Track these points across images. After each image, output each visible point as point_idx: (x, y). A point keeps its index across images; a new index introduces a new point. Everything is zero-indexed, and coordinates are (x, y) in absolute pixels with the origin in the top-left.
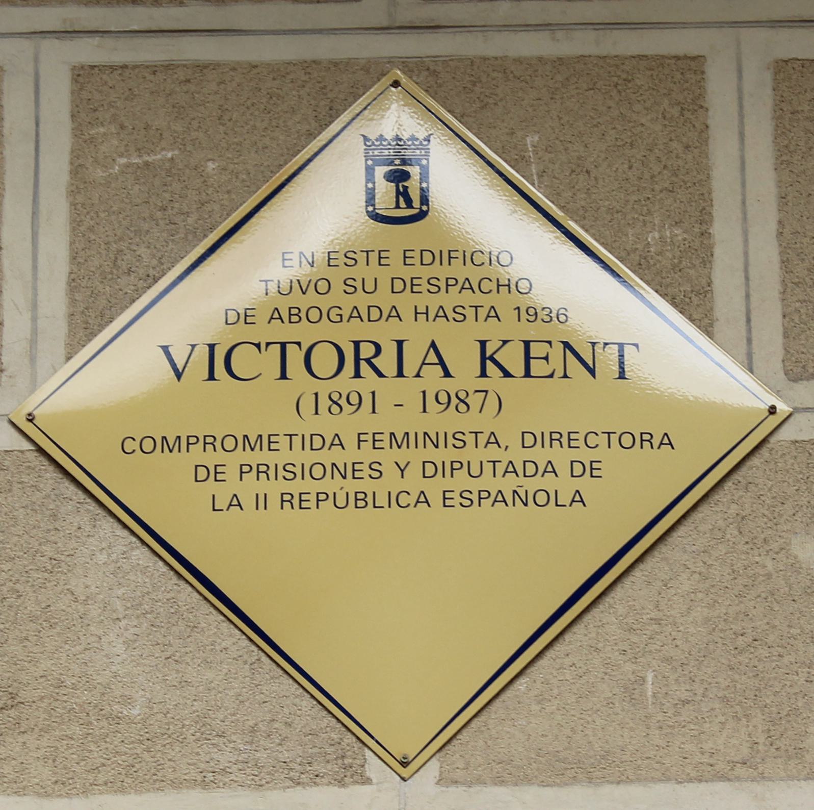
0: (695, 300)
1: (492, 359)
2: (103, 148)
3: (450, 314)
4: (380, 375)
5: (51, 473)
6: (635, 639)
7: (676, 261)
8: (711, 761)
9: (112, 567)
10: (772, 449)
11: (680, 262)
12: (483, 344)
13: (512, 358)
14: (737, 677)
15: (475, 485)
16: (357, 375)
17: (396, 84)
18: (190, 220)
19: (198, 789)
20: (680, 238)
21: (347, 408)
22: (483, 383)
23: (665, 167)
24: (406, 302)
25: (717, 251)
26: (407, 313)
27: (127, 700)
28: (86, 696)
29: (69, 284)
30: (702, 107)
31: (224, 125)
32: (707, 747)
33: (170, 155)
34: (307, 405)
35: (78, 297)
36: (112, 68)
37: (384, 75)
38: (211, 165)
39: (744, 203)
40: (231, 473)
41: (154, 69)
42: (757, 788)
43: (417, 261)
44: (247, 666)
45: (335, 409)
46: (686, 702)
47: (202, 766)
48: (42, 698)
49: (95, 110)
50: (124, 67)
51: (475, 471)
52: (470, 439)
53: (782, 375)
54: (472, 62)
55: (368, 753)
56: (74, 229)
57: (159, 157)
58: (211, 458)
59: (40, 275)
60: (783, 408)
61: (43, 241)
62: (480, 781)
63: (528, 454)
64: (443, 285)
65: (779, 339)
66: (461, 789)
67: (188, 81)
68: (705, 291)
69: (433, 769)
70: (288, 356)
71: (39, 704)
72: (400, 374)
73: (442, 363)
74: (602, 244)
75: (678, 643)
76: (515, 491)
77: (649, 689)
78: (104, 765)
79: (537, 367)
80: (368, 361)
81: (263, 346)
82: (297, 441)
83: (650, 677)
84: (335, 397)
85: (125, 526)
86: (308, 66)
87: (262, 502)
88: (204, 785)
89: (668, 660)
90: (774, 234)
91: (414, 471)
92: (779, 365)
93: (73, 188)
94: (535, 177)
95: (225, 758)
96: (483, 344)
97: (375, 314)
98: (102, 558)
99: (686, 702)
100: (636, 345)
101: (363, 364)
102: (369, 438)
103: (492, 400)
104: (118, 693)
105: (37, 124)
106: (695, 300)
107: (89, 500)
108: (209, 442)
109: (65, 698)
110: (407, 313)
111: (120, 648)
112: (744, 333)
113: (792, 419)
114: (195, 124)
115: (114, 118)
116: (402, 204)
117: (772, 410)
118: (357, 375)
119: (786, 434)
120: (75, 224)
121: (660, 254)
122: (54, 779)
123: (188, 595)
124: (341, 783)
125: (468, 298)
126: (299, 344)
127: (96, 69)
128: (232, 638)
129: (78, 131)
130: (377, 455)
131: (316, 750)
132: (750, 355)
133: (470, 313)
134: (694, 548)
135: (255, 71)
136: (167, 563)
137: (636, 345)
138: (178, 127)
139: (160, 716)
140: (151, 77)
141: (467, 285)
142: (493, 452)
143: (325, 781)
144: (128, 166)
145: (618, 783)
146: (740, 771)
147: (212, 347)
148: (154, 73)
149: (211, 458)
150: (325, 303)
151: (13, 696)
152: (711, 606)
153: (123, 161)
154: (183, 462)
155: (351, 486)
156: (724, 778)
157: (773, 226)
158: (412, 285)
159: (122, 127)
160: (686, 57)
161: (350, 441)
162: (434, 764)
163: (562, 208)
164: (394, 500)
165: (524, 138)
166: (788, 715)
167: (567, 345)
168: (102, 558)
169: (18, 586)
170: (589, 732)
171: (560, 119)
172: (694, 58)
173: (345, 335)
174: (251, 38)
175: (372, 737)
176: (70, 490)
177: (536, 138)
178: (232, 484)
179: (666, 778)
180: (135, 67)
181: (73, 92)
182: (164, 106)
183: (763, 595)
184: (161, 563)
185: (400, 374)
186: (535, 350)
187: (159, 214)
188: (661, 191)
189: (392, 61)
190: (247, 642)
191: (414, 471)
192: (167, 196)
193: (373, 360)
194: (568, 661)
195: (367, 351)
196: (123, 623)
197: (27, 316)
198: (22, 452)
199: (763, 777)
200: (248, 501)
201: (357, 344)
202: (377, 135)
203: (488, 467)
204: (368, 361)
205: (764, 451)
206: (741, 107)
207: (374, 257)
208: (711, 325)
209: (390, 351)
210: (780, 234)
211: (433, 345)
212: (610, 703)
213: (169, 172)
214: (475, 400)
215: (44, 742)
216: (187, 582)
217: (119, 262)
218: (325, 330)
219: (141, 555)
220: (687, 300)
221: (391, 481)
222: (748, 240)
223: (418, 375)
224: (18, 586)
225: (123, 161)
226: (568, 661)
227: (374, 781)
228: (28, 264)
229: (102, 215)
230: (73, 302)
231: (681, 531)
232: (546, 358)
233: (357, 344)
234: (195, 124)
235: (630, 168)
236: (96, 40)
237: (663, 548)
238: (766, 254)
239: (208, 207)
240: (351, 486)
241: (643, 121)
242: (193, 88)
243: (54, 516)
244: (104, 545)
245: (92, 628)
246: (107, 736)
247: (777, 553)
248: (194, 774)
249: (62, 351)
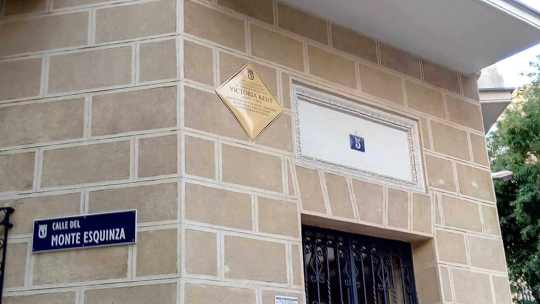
24: (253, 89)
149: (235, 101)
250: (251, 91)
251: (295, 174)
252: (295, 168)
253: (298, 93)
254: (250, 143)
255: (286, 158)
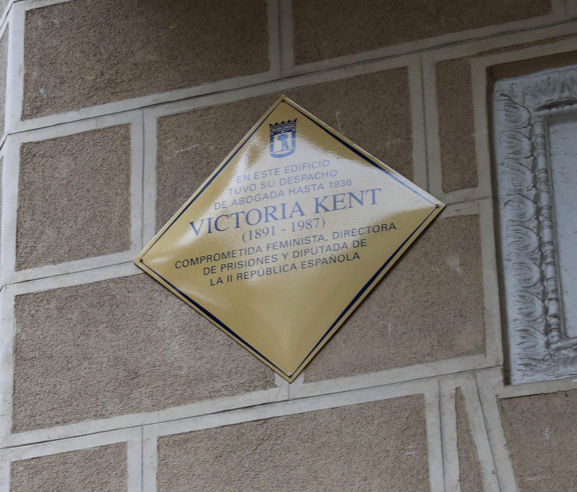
24: (285, 188)
26: (286, 192)
58: (210, 264)
108: (209, 258)
110: (286, 192)
128: (221, 336)
129: (160, 143)
142: (321, 243)
149: (210, 264)
195: (270, 210)
200: (224, 280)
214: (314, 223)
221: (281, 261)
250: (277, 202)
251: (498, 434)
252: (494, 414)
253: (544, 100)
254: (281, 390)
255: (449, 388)
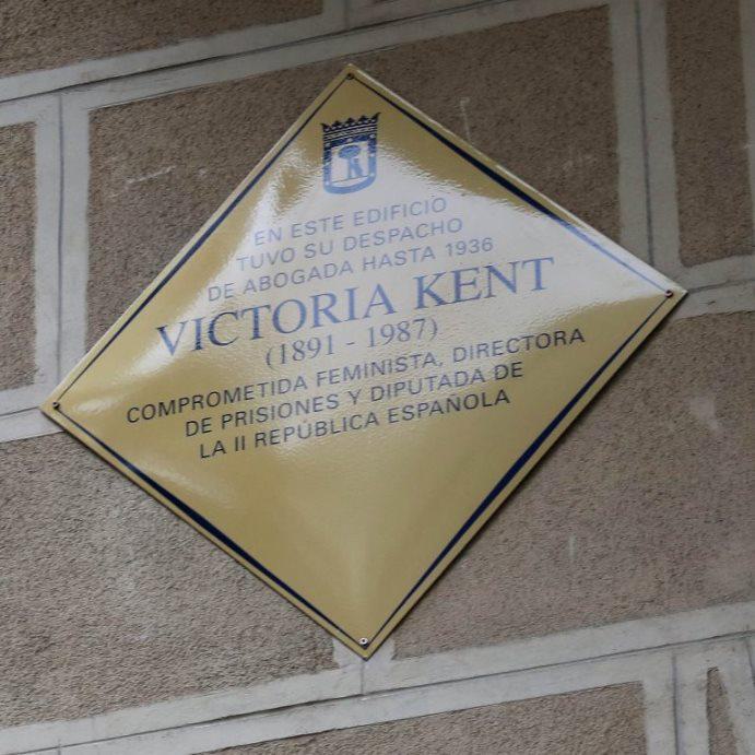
0: (605, 213)
1: (428, 291)
2: (114, 174)
3: (393, 260)
4: (335, 320)
5: (75, 449)
6: (556, 509)
7: (587, 182)
8: (625, 603)
9: (123, 519)
10: (671, 328)
11: (591, 183)
12: (420, 280)
13: (445, 288)
14: (645, 528)
15: (415, 400)
16: (317, 324)
17: (351, 76)
18: (186, 221)
19: (197, 694)
20: (591, 162)
21: (309, 354)
22: (421, 313)
23: (577, 105)
25: (622, 168)
26: (357, 265)
27: (138, 628)
28: (104, 630)
29: (88, 290)
30: (607, 48)
31: (212, 136)
32: (620, 592)
33: (168, 170)
34: (276, 357)
35: (95, 299)
36: (122, 107)
37: (340, 71)
38: (202, 172)
39: (644, 122)
40: (216, 423)
41: (156, 101)
42: (663, 621)
43: (365, 221)
44: (235, 584)
45: (299, 356)
46: (601, 557)
47: (200, 674)
48: (70, 637)
49: (109, 144)
50: (131, 104)
51: (415, 388)
52: (410, 362)
53: (679, 263)
54: (414, 47)
55: (335, 642)
56: (92, 245)
57: (160, 173)
58: (198, 414)
59: (64, 287)
60: (680, 291)
61: (66, 261)
62: (429, 651)
63: (459, 367)
64: (386, 236)
65: (676, 233)
66: (413, 660)
67: (182, 106)
68: (612, 204)
69: (389, 648)
70: (475, 168)
71: (66, 643)
72: (352, 317)
73: (386, 302)
74: (526, 180)
75: (596, 506)
76: (449, 400)
77: (571, 549)
78: (119, 686)
79: (467, 292)
80: (326, 311)
81: (239, 314)
82: (268, 388)
83: (572, 540)
84: (299, 345)
85: (134, 483)
86: (279, 75)
87: (240, 444)
88: (201, 689)
89: (587, 523)
90: (670, 143)
91: (364, 398)
92: (677, 255)
93: (91, 211)
94: (468, 133)
95: (216, 666)
96: (420, 280)
97: (331, 270)
98: (116, 512)
99: (601, 557)
100: (551, 259)
101: (322, 314)
102: (327, 375)
103: (429, 326)
104: (130, 623)
105: (62, 164)
106: (605, 213)
107: (105, 466)
108: (197, 401)
109: (88, 635)
110: (357, 265)
111: (131, 586)
112: (645, 232)
113: (688, 300)
114: (189, 140)
115: (125, 147)
116: (354, 175)
117: (670, 295)
118: (317, 324)
119: (683, 313)
120: (93, 241)
121: (573, 178)
122: (80, 704)
123: (186, 531)
124: (313, 670)
125: (408, 244)
126: (268, 307)
127: (201, 98)
128: (223, 562)
130: (335, 389)
131: (292, 646)
132: (651, 251)
133: (409, 256)
134: (607, 424)
135: (236, 88)
136: (168, 509)
137: (551, 259)
138: (175, 145)
139: (163, 638)
140: (153, 109)
141: (407, 233)
142: (430, 370)
143: (300, 670)
144: (134, 185)
145: (545, 635)
146: (648, 608)
147: (198, 321)
148: (156, 105)
149: (198, 414)
150: (289, 269)
151: (46, 639)
152: (621, 471)
153: (131, 181)
154: (178, 420)
155: (313, 418)
156: (635, 617)
157: (669, 137)
158: (361, 242)
159: (131, 154)
160: (592, 9)
161: (311, 381)
162: (391, 643)
163: (490, 155)
164: (349, 424)
165: (458, 102)
166: (689, 554)
167: (491, 269)
168: (116, 512)
169: (49, 548)
170: (519, 595)
171: (488, 80)
172: (599, 8)
173: (304, 293)
174: (232, 60)
175: (337, 628)
176: (89, 460)
177: (468, 100)
178: (217, 433)
179: (586, 623)
180: (140, 103)
181: (90, 132)
182: (163, 131)
183: (667, 454)
184: (164, 509)
185: (352, 317)
186: (465, 278)
187: (160, 220)
188: (574, 125)
189: (347, 58)
190: (234, 564)
191: (364, 398)
192: (167, 204)
193: (330, 310)
194: (502, 537)
195: (324, 302)
196: (133, 565)
197: (55, 322)
198: (52, 435)
199: (669, 611)
200: (229, 446)
201: (316, 298)
202: (346, 120)
203: (425, 383)
204: (326, 311)
205: (665, 332)
206: (639, 42)
207: (330, 223)
208: (618, 231)
209: (343, 300)
210: (675, 144)
211: (379, 288)
212: (537, 568)
213: (169, 185)
214: (414, 329)
215: (71, 674)
216: (187, 523)
217: (129, 266)
218: (289, 292)
219: (147, 505)
220: (598, 214)
222: (647, 152)
223: (366, 316)
224: (49, 548)
225: (131, 181)
226: (502, 537)
227: (341, 664)
228: (55, 281)
229: (115, 229)
230: (91, 305)
231: (596, 412)
232: (473, 283)
233: (316, 298)
234: (189, 140)
235: (548, 110)
236: (109, 86)
237: (582, 429)
238: (664, 163)
239: (201, 207)
240: (313, 418)
241: (558, 69)
242: (186, 111)
243: (78, 485)
244: (118, 501)
245: (108, 572)
246: (122, 661)
247: (678, 416)
248: (193, 682)
249: (82, 346)
